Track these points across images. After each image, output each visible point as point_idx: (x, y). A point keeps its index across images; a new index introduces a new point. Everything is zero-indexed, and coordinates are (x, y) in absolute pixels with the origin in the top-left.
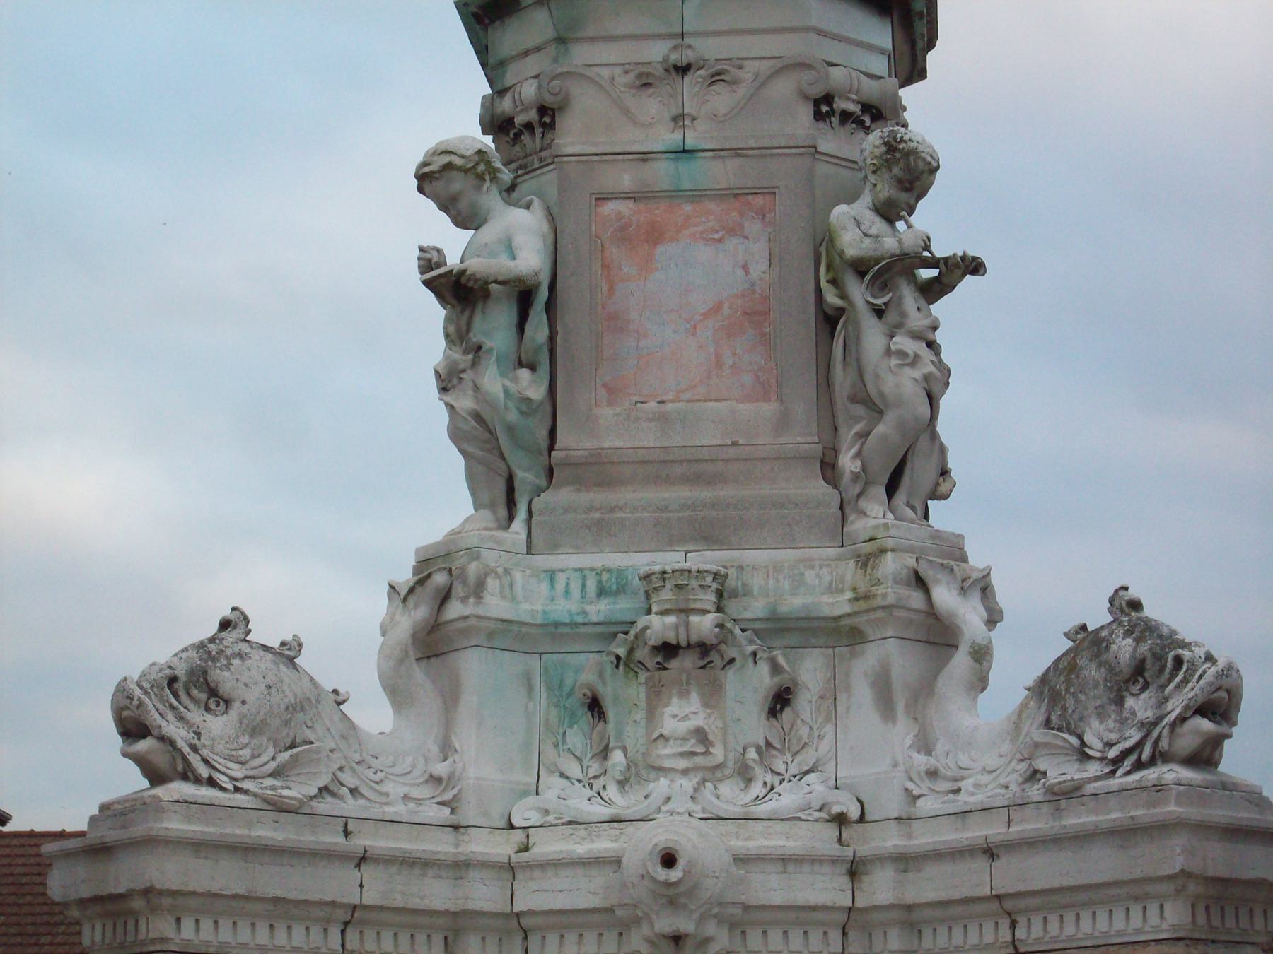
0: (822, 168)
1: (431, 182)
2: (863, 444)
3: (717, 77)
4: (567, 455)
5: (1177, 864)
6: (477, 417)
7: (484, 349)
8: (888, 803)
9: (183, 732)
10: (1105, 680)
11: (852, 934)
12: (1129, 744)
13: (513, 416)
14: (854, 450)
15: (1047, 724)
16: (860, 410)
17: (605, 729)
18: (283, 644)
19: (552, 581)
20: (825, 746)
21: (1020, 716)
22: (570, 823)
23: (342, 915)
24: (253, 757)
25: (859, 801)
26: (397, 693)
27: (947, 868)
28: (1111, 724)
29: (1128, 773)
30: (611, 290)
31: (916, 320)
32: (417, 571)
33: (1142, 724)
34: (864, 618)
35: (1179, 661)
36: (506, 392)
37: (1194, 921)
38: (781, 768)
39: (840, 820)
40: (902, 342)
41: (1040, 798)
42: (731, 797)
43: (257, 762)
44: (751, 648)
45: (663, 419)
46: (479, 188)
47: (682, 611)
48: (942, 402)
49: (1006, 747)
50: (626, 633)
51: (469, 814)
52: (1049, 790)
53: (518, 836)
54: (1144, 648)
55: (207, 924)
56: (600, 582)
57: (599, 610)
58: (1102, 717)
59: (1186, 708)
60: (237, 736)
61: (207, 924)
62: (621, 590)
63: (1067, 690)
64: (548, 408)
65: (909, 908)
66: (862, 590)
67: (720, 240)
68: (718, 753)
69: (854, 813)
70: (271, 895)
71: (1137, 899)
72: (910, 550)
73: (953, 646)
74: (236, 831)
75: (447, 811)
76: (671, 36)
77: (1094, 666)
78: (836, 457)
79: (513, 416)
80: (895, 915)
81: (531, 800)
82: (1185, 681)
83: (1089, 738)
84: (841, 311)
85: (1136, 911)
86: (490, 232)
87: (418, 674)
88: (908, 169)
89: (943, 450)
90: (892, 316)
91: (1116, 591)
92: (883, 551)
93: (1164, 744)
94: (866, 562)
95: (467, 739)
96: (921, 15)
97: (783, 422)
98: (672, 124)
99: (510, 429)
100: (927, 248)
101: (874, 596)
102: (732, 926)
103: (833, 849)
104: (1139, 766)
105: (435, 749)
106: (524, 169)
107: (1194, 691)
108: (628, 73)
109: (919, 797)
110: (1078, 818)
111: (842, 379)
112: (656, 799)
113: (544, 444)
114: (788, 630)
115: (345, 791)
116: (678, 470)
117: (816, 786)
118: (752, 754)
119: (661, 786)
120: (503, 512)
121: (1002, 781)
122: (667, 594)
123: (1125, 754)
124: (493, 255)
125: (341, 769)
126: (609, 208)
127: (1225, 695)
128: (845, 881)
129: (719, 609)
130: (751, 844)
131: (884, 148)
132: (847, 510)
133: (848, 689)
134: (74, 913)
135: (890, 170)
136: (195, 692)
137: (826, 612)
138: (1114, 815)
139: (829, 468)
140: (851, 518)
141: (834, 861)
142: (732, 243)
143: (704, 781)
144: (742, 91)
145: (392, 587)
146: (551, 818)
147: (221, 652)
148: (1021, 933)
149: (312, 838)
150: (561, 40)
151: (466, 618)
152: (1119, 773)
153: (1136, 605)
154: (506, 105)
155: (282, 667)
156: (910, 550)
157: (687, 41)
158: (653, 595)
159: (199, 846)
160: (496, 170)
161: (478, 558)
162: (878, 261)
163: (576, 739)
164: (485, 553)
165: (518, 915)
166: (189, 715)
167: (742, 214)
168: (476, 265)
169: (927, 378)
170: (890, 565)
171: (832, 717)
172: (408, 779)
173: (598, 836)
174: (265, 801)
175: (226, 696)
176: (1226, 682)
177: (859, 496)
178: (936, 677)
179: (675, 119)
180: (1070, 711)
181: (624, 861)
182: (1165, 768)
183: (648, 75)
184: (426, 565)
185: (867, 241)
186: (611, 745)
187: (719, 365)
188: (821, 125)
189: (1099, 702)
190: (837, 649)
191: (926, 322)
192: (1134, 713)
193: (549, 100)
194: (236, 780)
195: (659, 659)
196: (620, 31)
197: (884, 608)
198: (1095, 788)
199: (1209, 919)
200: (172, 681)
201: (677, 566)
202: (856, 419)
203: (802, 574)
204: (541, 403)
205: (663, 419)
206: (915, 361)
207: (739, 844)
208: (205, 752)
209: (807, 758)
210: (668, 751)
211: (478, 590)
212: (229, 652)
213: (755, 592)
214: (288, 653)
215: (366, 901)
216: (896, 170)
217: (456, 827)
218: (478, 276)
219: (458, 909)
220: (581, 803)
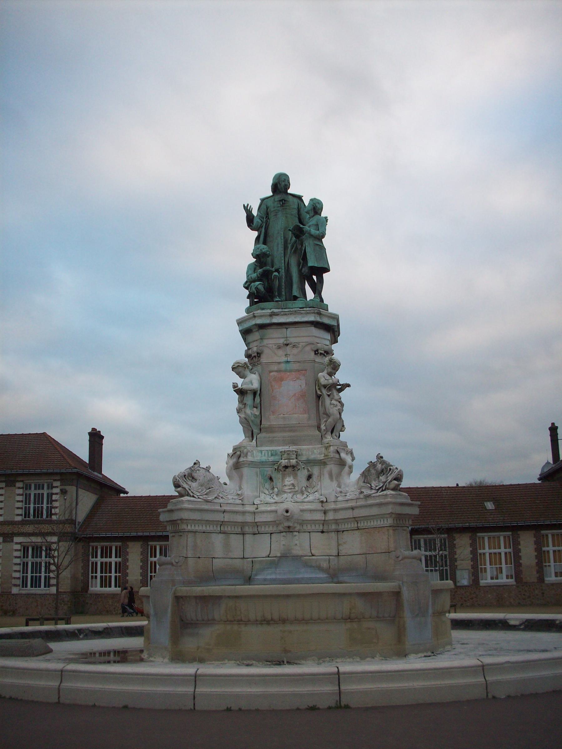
0: (316, 365)
3: (294, 346)
5: (390, 511)
6: (245, 419)
8: (332, 499)
9: (187, 486)
11: (324, 525)
12: (380, 486)
13: (253, 418)
14: (324, 425)
15: (364, 482)
16: (325, 416)
18: (207, 467)
19: (261, 453)
20: (319, 487)
21: (358, 480)
22: (266, 503)
23: (220, 523)
24: (202, 491)
26: (230, 477)
28: (377, 482)
29: (380, 492)
30: (273, 390)
31: (336, 397)
32: (233, 451)
33: (383, 482)
34: (326, 460)
35: (390, 469)
36: (251, 413)
37: (394, 523)
38: (310, 491)
39: (322, 502)
40: (334, 402)
42: (299, 497)
43: (202, 492)
44: (303, 466)
45: (284, 418)
46: (245, 370)
48: (342, 414)
49: (356, 487)
51: (246, 502)
52: (365, 496)
53: (256, 506)
54: (383, 466)
55: (193, 526)
56: (271, 453)
57: (272, 459)
58: (375, 480)
59: (392, 479)
61: (193, 526)
62: (276, 454)
64: (260, 416)
65: (336, 520)
67: (295, 380)
68: (297, 488)
69: (325, 501)
71: (382, 518)
72: (336, 445)
73: (344, 465)
74: (198, 506)
75: (241, 501)
76: (285, 338)
77: (373, 470)
78: (320, 426)
79: (253, 418)
80: (333, 521)
81: (258, 499)
83: (372, 485)
84: (321, 395)
85: (382, 520)
86: (247, 380)
87: (234, 472)
88: (334, 365)
89: (343, 421)
90: (331, 396)
91: (378, 454)
92: (330, 446)
93: (387, 486)
94: (327, 448)
95: (244, 486)
96: (336, 331)
97: (309, 419)
98: (285, 356)
99: (252, 421)
100: (338, 382)
102: (300, 524)
103: (321, 508)
104: (383, 491)
105: (238, 488)
106: (254, 365)
107: (393, 475)
109: (338, 497)
110: (370, 502)
112: (284, 498)
113: (259, 424)
114: (311, 462)
115: (220, 497)
116: (287, 429)
117: (317, 495)
118: (304, 489)
119: (285, 496)
120: (251, 438)
121: (355, 494)
122: (285, 456)
124: (248, 384)
125: (219, 493)
126: (272, 374)
128: (323, 515)
129: (296, 459)
130: (304, 507)
131: (329, 361)
132: (323, 437)
133: (323, 474)
134: (165, 523)
135: (330, 365)
136: (189, 478)
139: (319, 428)
140: (324, 439)
141: (321, 510)
142: (298, 381)
143: (294, 494)
145: (228, 454)
146: (262, 502)
147: (194, 469)
148: (359, 525)
149: (214, 508)
150: (261, 339)
151: (244, 461)
153: (382, 457)
154: (250, 352)
156: (336, 445)
157: (288, 339)
159: (191, 510)
160: (248, 366)
161: (246, 448)
162: (329, 385)
163: (267, 486)
164: (247, 447)
165: (256, 522)
166: (188, 483)
168: (244, 387)
169: (339, 409)
170: (332, 449)
171: (320, 481)
172: (232, 495)
174: (204, 500)
176: (400, 473)
177: (325, 434)
178: (341, 472)
179: (286, 355)
181: (278, 512)
182: (387, 491)
183: (280, 346)
184: (235, 449)
185: (326, 381)
186: (274, 487)
187: (296, 406)
188: (316, 356)
189: (374, 478)
191: (339, 397)
192: (381, 480)
193: (259, 351)
197: (330, 458)
199: (397, 522)
200: (185, 476)
201: (288, 450)
202: (324, 418)
203: (314, 451)
204: (259, 415)
205: (284, 418)
206: (336, 406)
207: (301, 507)
208: (192, 490)
211: (246, 455)
212: (196, 469)
213: (304, 455)
214: (208, 469)
215: (225, 520)
216: (331, 366)
217: (243, 504)
219: (244, 521)
220: (268, 499)
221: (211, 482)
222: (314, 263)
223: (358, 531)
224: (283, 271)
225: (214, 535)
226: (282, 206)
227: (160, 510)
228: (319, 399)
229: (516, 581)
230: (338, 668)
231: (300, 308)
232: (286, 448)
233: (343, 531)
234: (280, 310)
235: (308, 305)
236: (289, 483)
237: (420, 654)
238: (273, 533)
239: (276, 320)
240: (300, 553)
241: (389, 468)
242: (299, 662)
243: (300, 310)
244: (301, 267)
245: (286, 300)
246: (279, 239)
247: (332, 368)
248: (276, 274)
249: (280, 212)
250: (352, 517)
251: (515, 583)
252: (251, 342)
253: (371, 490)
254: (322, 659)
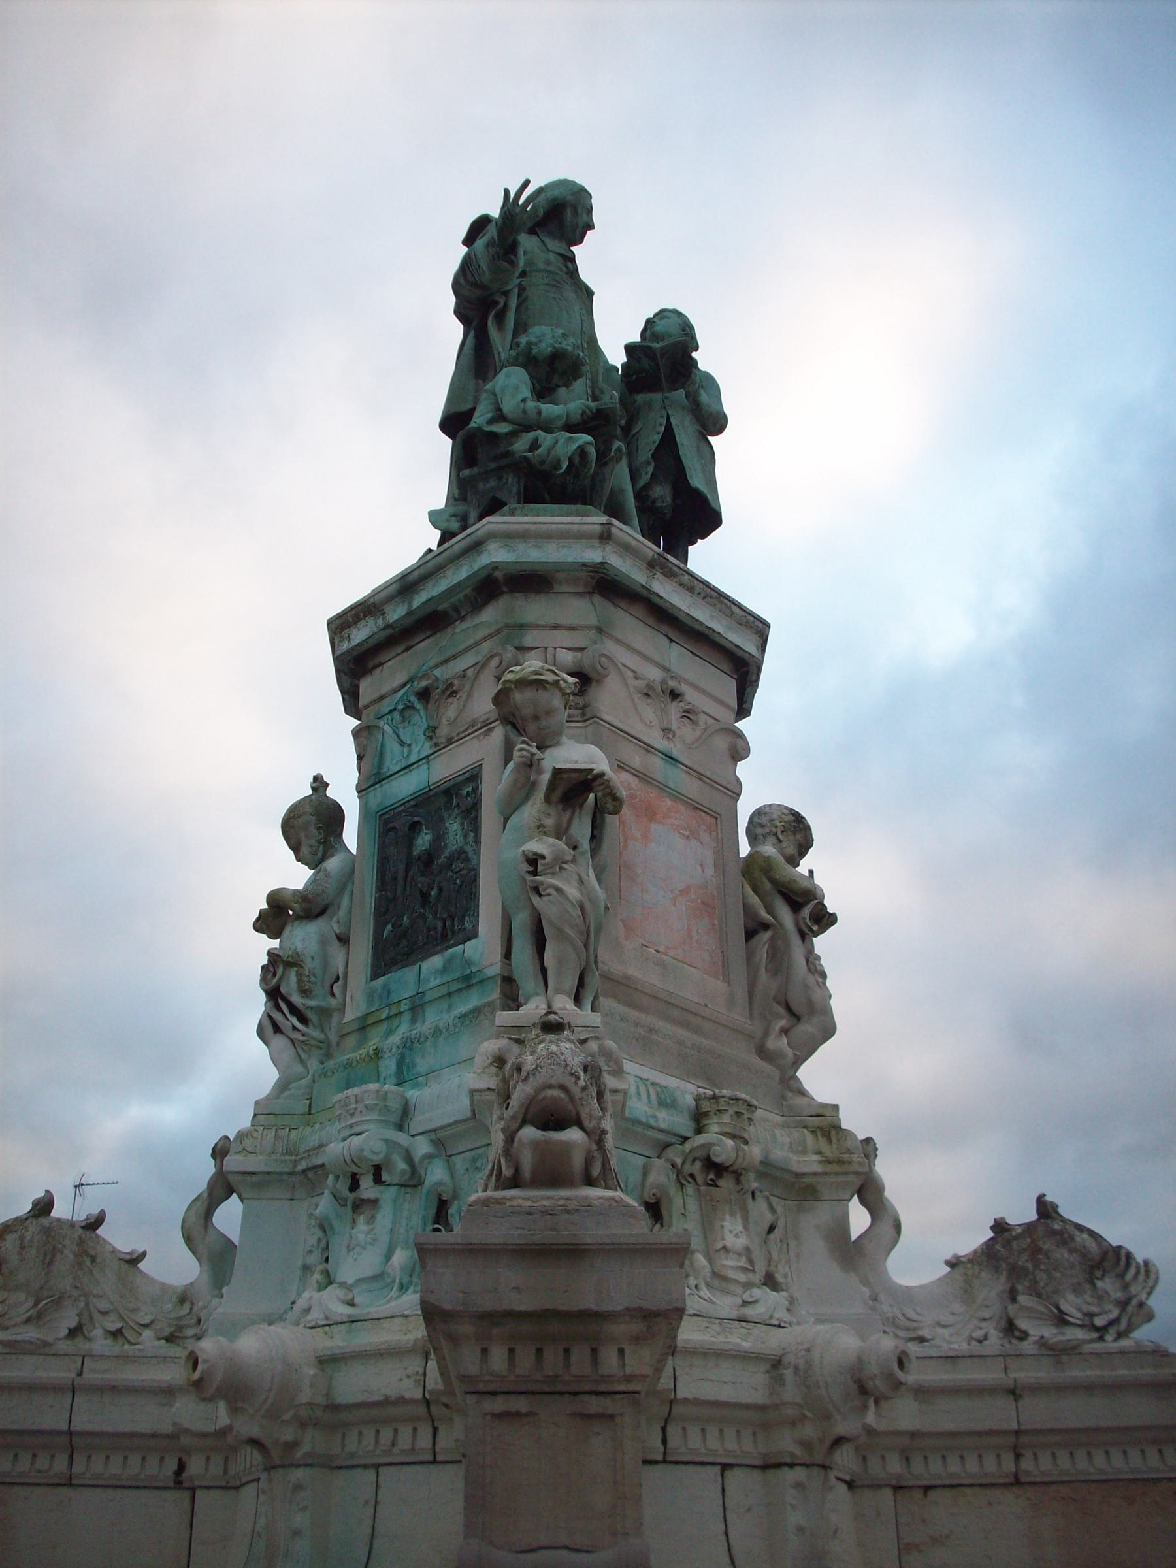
1: (537, 690)
41: (1035, 1352)
58: (1077, 1290)
63: (1036, 1267)
104: (1119, 1336)
108: (637, 679)
110: (1078, 1372)
137: (796, 1168)
158: (715, 1117)
173: (731, 1333)
189: (1075, 1280)
196: (636, 645)
198: (1093, 1349)
210: (729, 1263)
216: (798, 836)
218: (611, 784)
223: (1015, 1489)
233: (927, 1489)
250: (65, 1428)
252: (537, 627)
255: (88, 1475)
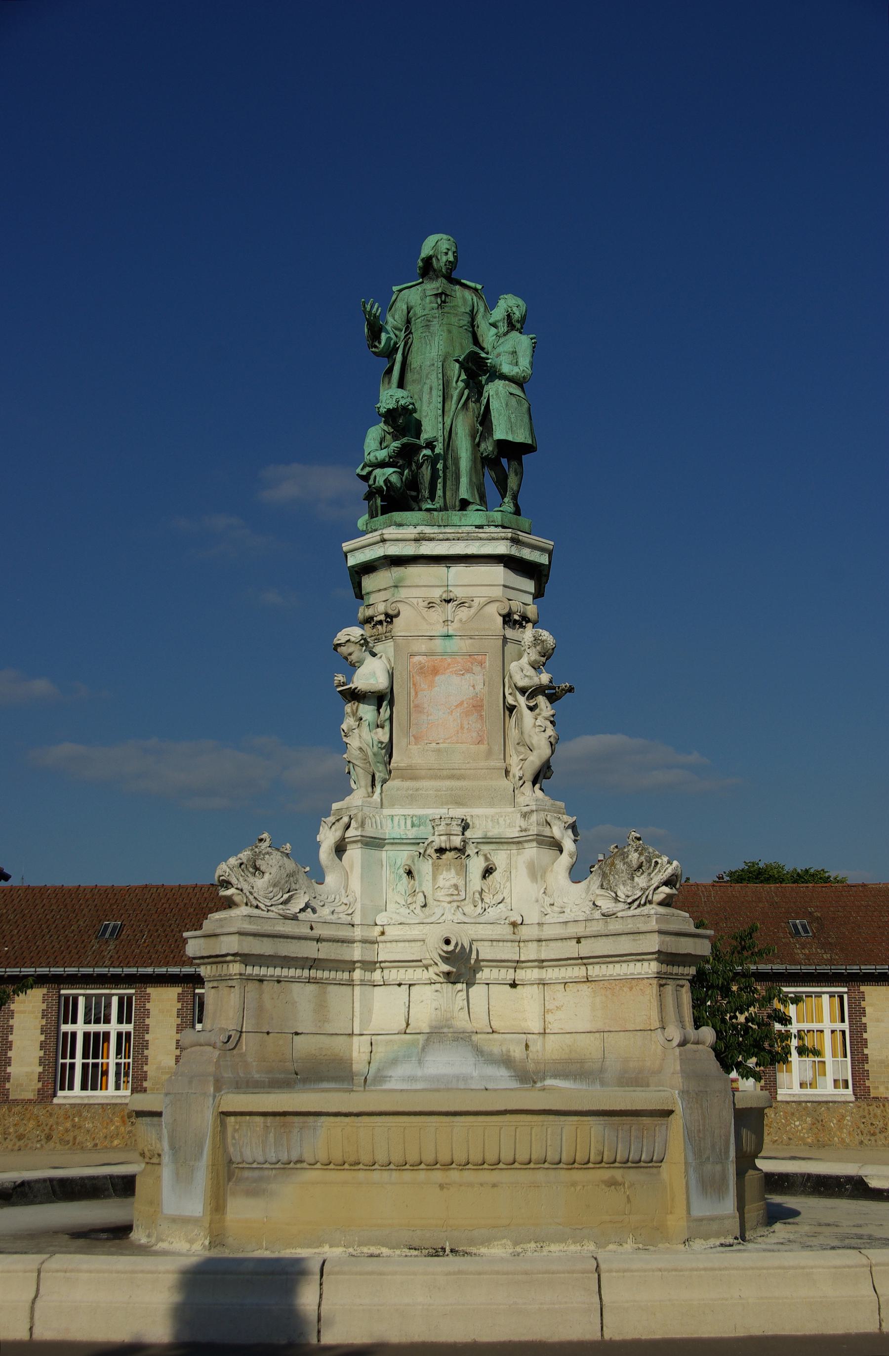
2: (523, 764)
4: (397, 766)
7: (363, 719)
10: (626, 870)
12: (636, 897)
15: (602, 887)
17: (414, 884)
19: (392, 820)
22: (401, 924)
25: (521, 916)
27: (559, 944)
29: (636, 908)
39: (514, 925)
47: (447, 835)
50: (424, 843)
56: (412, 821)
57: (412, 833)
60: (268, 888)
63: (610, 873)
66: (524, 827)
67: (463, 675)
69: (520, 922)
70: (283, 955)
74: (267, 928)
81: (384, 913)
82: (659, 871)
83: (619, 893)
84: (515, 707)
101: (529, 830)
104: (639, 906)
110: (614, 926)
111: (513, 733)
120: (370, 790)
122: (442, 828)
123: (634, 901)
126: (416, 659)
127: (675, 878)
135: (535, 647)
138: (630, 926)
142: (467, 676)
144: (473, 610)
149: (298, 931)
152: (632, 909)
155: (285, 858)
167: (472, 663)
174: (280, 915)
175: (263, 871)
180: (611, 882)
185: (527, 679)
187: (462, 728)
190: (512, 851)
192: (638, 884)
193: (391, 612)
194: (268, 906)
195: (438, 855)
208: (255, 895)
209: (499, 897)
212: (264, 852)
216: (538, 648)
221: (291, 878)
222: (507, 433)
223: (588, 984)
224: (441, 445)
225: (296, 987)
226: (440, 306)
227: (185, 934)
228: (512, 713)
229: (855, 1094)
230: (596, 1259)
231: (478, 527)
232: (443, 811)
234: (436, 530)
235: (492, 522)
236: (448, 884)
237: (712, 1239)
238: (415, 984)
239: (427, 549)
240: (469, 1027)
241: (653, 861)
242: (473, 1250)
243: (477, 530)
244: (477, 440)
245: (445, 508)
246: (433, 377)
247: (540, 653)
248: (427, 452)
249: (435, 322)
251: (853, 1098)
253: (615, 903)
254: (521, 1245)
255: (391, 980)
